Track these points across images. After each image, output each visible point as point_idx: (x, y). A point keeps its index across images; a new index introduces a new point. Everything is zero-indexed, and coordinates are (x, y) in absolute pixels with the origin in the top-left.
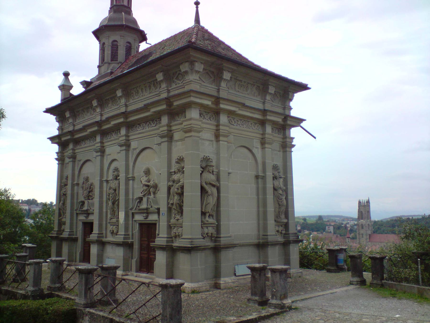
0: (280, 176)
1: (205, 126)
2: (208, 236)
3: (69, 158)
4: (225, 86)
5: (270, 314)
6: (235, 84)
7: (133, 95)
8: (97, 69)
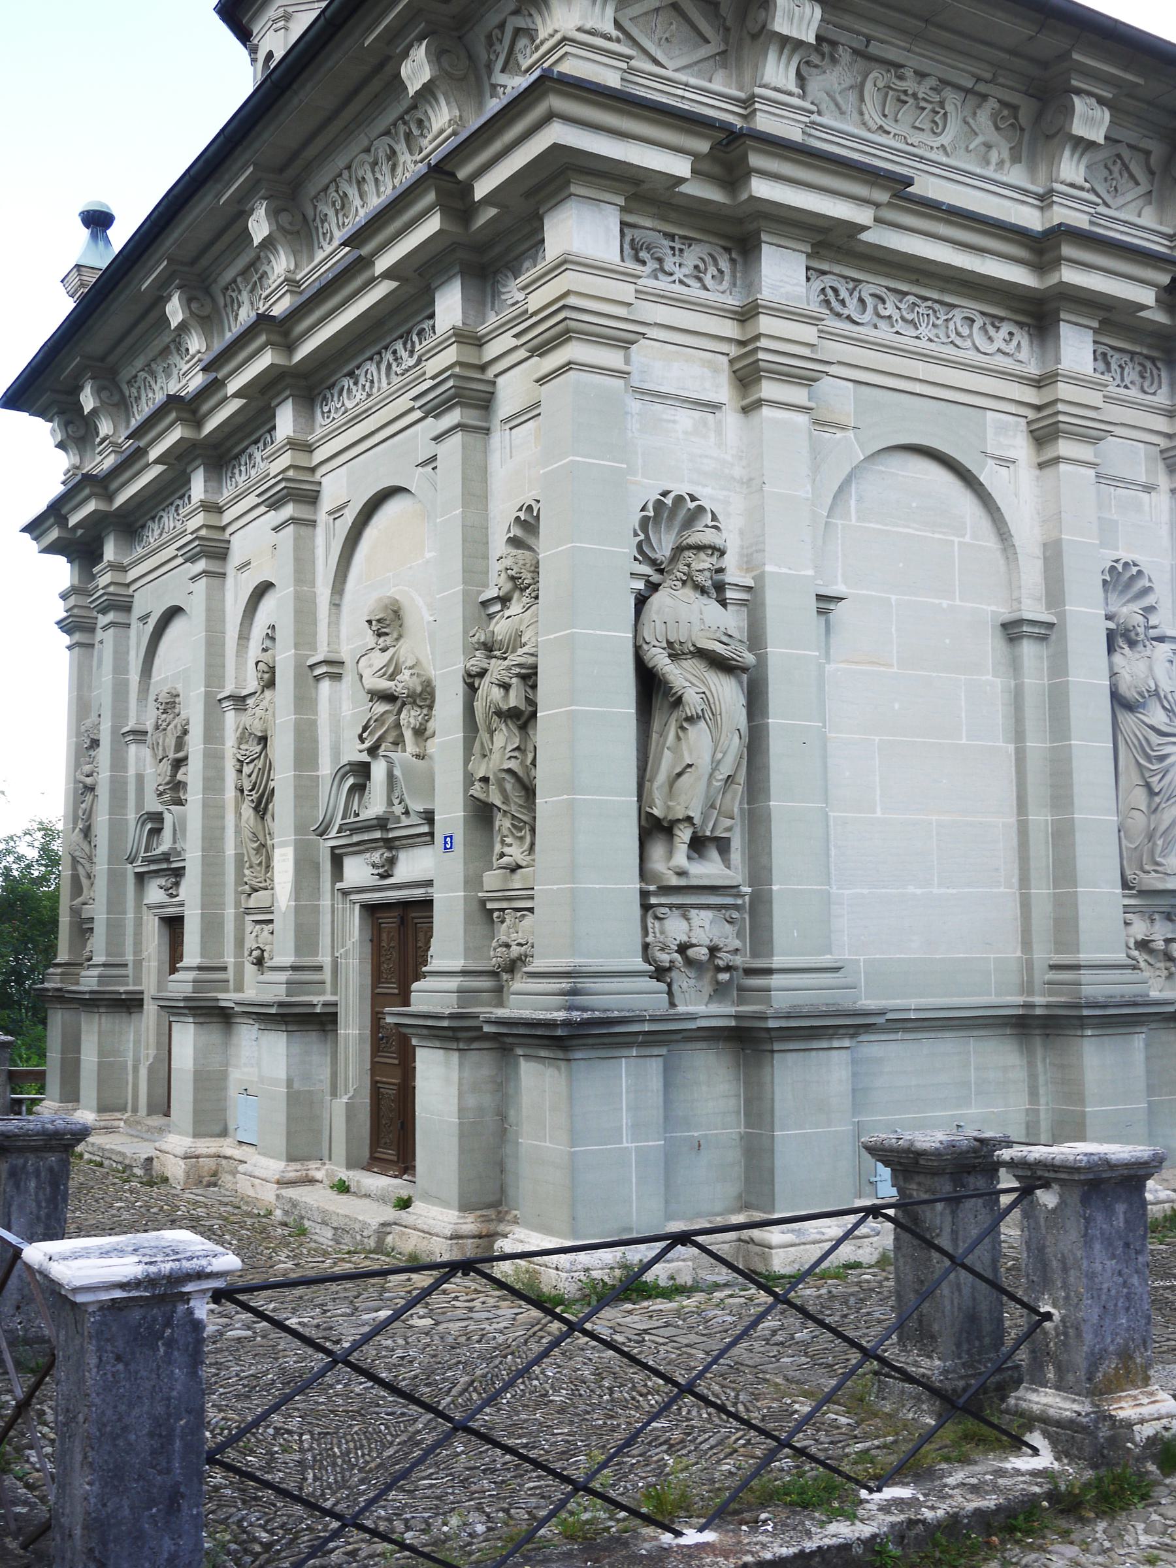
0: (1153, 633)
2: (689, 962)
4: (792, 86)
6: (862, 84)
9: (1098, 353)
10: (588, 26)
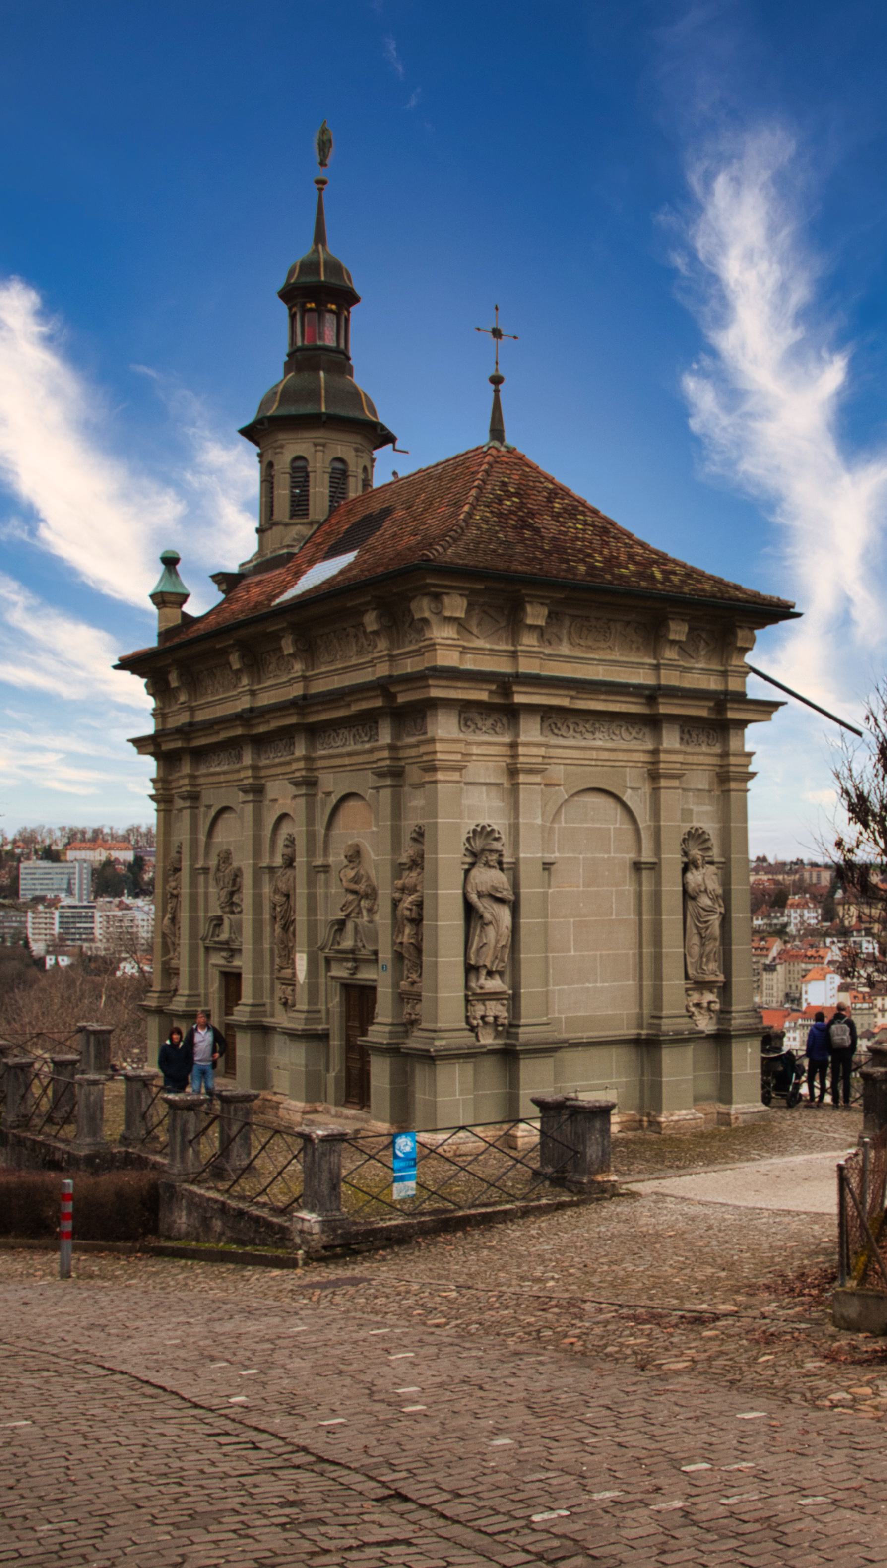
3: (183, 798)
8: (255, 537)
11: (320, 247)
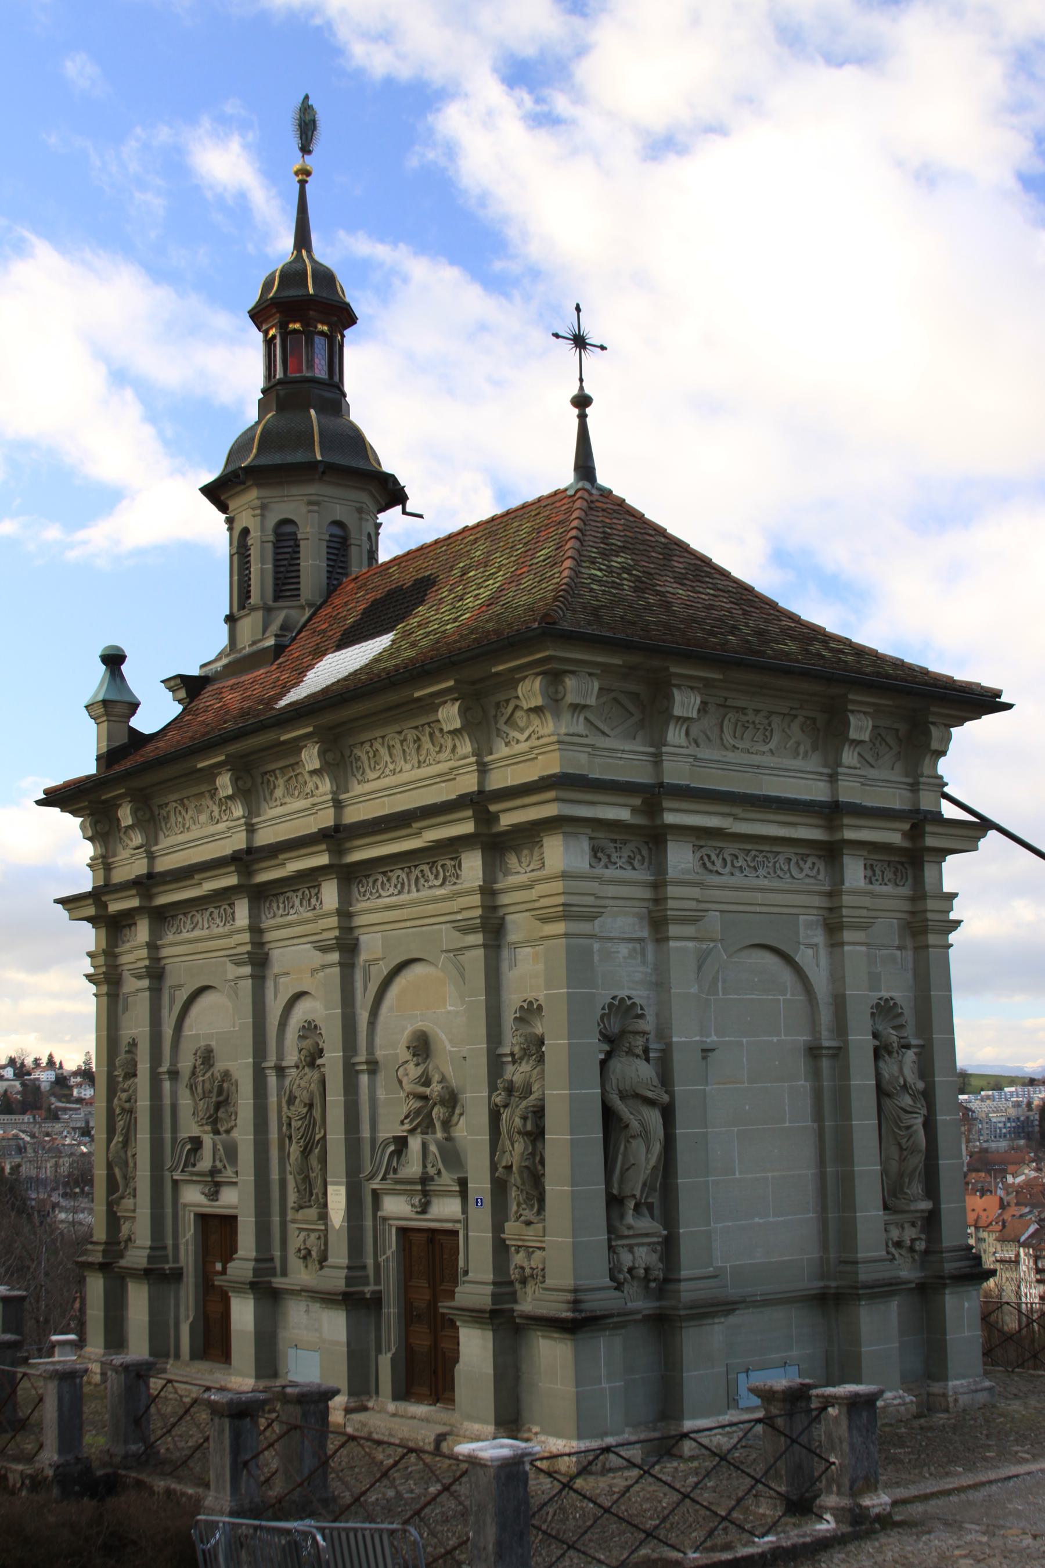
1: (612, 890)
3: (139, 977)
5: (812, 1542)
7: (359, 763)
8: (225, 628)
9: (868, 866)
10: (571, 731)
11: (304, 253)
